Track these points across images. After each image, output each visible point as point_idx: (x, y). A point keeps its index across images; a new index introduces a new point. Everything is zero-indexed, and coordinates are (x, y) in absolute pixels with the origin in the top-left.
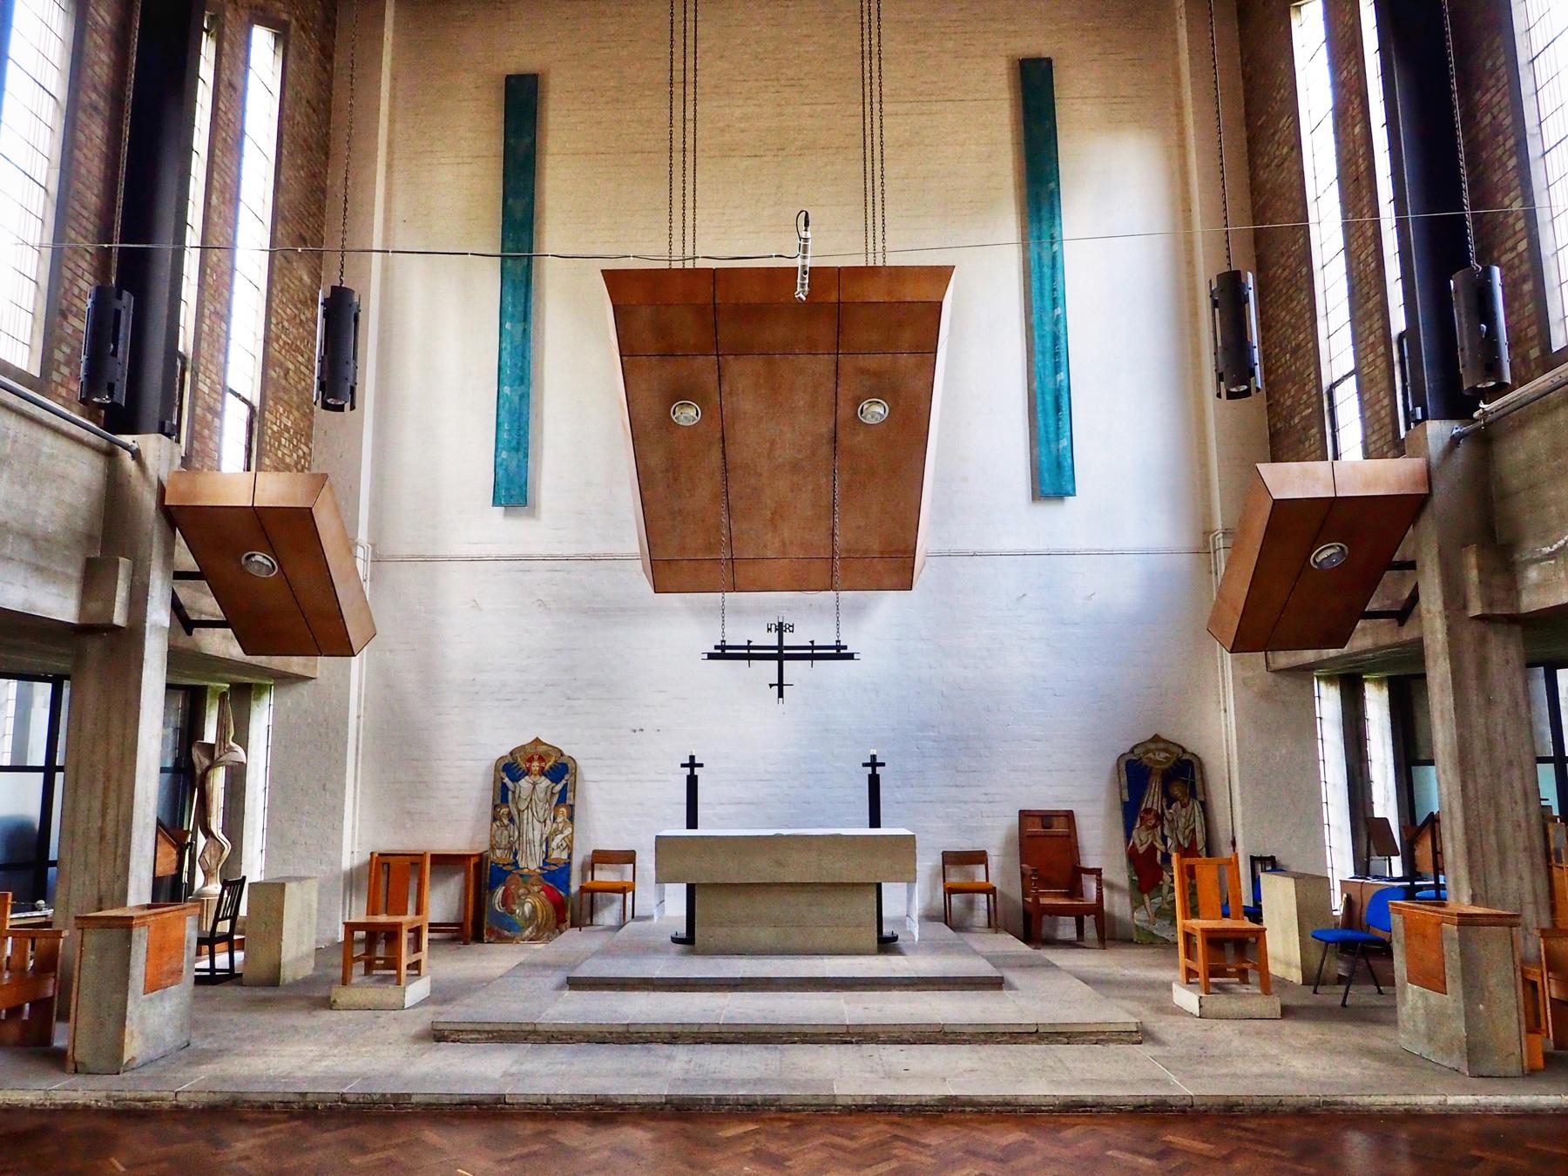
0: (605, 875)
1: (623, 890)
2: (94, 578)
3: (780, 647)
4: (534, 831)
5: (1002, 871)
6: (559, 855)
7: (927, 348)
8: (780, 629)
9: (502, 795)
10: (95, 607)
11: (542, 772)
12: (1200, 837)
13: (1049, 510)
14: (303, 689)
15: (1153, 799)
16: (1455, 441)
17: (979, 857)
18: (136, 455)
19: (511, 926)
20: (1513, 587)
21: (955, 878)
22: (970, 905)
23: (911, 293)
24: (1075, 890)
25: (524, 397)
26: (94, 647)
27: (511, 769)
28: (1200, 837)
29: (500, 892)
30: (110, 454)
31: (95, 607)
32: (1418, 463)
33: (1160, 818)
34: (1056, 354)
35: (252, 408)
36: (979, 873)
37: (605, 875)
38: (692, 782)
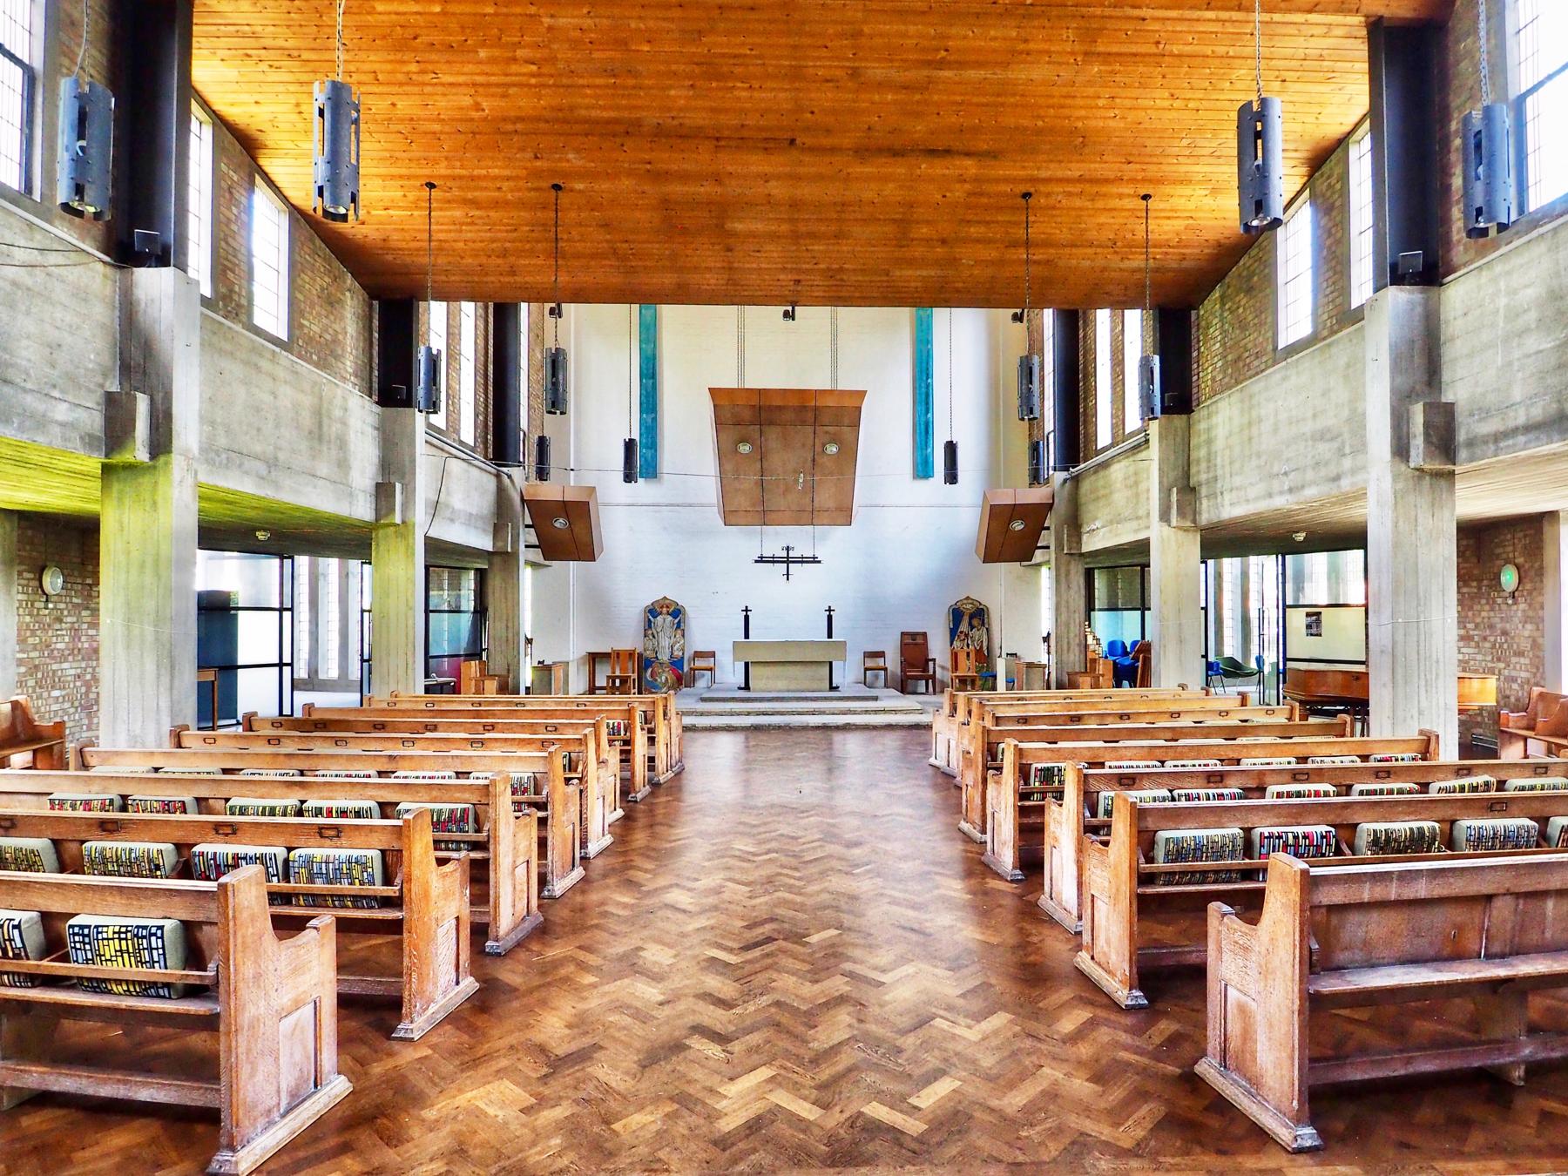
0: (699, 663)
1: (711, 669)
2: (498, 530)
3: (788, 557)
4: (665, 642)
5: (893, 662)
6: (678, 653)
7: (856, 424)
8: (788, 549)
9: (649, 625)
10: (500, 544)
11: (668, 613)
12: (985, 644)
13: (922, 483)
14: (545, 570)
15: (964, 627)
16: (1065, 481)
17: (881, 654)
18: (510, 477)
19: (656, 687)
20: (1079, 542)
21: (870, 663)
22: (877, 677)
23: (847, 403)
24: (926, 669)
25: (654, 420)
26: (497, 560)
27: (653, 611)
28: (985, 644)
29: (650, 670)
30: (498, 476)
31: (500, 544)
32: (1049, 490)
33: (967, 635)
34: (927, 404)
35: (29, 71)
36: (880, 662)
37: (699, 663)
38: (747, 618)
